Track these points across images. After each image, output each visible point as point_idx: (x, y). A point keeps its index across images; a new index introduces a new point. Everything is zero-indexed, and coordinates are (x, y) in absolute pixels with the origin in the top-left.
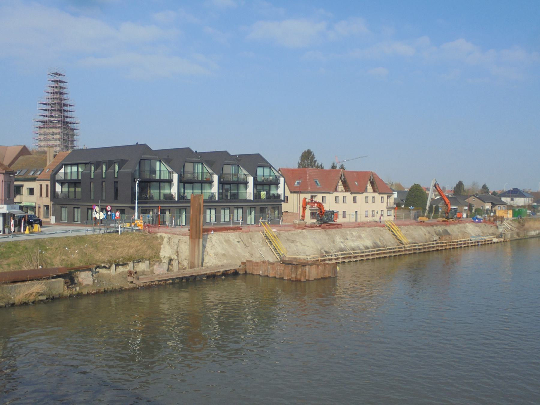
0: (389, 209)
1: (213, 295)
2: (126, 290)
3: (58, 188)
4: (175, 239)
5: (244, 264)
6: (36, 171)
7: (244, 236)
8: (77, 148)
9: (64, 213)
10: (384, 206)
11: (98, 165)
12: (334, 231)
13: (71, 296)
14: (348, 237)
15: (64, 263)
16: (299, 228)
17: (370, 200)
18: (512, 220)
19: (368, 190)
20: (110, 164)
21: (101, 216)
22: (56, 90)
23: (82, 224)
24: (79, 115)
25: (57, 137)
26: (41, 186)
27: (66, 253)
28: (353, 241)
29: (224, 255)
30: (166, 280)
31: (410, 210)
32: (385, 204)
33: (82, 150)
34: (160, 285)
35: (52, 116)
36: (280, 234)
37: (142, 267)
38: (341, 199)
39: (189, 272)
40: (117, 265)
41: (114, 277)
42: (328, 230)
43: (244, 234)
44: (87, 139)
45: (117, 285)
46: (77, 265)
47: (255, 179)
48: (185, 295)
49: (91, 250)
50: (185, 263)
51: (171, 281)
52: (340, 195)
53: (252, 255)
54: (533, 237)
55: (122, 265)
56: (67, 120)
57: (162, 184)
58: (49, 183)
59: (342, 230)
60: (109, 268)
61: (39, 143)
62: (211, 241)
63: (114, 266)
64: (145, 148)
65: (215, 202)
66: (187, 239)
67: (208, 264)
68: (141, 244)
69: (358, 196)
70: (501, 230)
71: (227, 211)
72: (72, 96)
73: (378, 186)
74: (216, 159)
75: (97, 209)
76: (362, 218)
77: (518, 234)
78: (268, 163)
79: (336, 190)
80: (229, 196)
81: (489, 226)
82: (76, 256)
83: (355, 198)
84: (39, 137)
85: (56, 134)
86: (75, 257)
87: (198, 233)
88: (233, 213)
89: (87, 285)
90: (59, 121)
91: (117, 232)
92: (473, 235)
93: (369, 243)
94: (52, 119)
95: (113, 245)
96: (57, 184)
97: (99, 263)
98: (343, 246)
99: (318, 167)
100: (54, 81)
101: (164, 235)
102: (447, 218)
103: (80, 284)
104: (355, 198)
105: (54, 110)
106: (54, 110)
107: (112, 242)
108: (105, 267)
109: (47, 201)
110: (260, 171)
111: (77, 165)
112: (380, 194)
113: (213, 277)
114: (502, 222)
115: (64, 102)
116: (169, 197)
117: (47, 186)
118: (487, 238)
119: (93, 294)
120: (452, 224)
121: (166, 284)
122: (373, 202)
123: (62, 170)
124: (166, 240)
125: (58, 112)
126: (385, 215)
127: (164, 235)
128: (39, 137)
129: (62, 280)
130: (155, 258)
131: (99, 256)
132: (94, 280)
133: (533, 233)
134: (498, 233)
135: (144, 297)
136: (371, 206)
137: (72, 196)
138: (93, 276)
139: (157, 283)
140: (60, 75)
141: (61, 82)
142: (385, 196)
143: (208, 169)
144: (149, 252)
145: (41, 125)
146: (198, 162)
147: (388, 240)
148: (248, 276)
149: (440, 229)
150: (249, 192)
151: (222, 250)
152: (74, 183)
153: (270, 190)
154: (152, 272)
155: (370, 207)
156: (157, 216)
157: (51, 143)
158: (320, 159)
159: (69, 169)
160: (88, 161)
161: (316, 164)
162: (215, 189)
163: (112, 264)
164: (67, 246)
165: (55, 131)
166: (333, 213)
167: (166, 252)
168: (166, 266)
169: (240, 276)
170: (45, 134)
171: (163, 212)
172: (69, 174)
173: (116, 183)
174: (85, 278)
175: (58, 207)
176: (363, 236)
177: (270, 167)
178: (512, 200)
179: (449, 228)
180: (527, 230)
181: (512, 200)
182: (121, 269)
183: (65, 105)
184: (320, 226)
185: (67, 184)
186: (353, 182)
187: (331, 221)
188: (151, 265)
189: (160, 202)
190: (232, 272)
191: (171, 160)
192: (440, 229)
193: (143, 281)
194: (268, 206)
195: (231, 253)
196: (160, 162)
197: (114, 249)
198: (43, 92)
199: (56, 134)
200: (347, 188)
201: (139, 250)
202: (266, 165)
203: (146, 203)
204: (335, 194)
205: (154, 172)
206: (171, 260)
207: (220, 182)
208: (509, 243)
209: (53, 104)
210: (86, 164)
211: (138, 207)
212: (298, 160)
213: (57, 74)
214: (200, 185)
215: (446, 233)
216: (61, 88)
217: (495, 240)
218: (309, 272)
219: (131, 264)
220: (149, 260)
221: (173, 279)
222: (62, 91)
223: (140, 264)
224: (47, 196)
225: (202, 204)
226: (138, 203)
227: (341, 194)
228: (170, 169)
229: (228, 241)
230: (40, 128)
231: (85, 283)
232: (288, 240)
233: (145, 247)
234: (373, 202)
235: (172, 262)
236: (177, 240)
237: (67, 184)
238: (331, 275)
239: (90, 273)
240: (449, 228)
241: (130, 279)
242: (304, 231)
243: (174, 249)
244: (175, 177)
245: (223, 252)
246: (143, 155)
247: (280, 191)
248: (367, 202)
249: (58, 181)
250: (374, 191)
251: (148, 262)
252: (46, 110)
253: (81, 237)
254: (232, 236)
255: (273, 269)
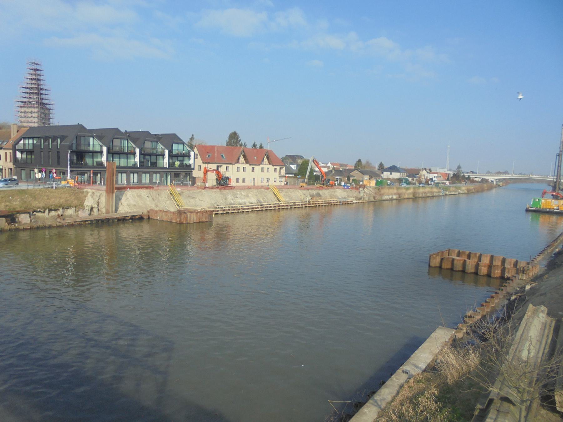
0: (281, 177)
1: (128, 233)
2: (54, 227)
3: (19, 155)
4: (97, 194)
5: (148, 212)
6: (3, 142)
7: (153, 193)
8: (52, 125)
9: (23, 173)
10: (277, 175)
11: (46, 139)
12: (227, 191)
13: (10, 230)
14: (238, 196)
15: (8, 207)
16: (201, 188)
17: (265, 170)
18: (373, 188)
19: (264, 163)
20: (54, 139)
21: (39, 176)
22: (34, 77)
23: (27, 181)
24: (53, 97)
25: (36, 115)
26: (6, 153)
27: (10, 201)
28: (241, 199)
29: (135, 205)
30: (86, 221)
31: (298, 178)
32: (278, 174)
33: (56, 126)
34: (81, 224)
35: (30, 98)
36: (183, 192)
37: (70, 212)
38: (241, 169)
39: (103, 216)
40: (50, 210)
41: (47, 219)
42: (222, 191)
43: (154, 191)
44: (61, 117)
45: (48, 223)
46: (18, 209)
47: (170, 152)
48: (103, 233)
49: (30, 199)
50: (104, 210)
51: (89, 222)
52: (265, 167)
53: (157, 206)
54: (387, 200)
55: (55, 210)
56: (44, 101)
57: (94, 154)
58: (11, 151)
59: (234, 191)
60: (44, 212)
61: (20, 119)
62: (126, 195)
63: (47, 211)
64: (81, 127)
65: (138, 168)
66: (105, 193)
67: (121, 212)
68: (70, 196)
69: (256, 167)
70: (362, 195)
71: (148, 175)
72: (48, 82)
73: (271, 159)
74: (138, 138)
75: (36, 170)
76: (258, 183)
77: (374, 198)
78: (181, 140)
79: (238, 161)
80: (149, 163)
81: (354, 191)
82: (18, 203)
83: (253, 169)
84: (21, 114)
85: (34, 112)
86: (16, 204)
87: (115, 190)
88: (152, 177)
89: (26, 223)
90: (37, 102)
91: (53, 187)
92: (340, 197)
93: (254, 200)
94: (31, 100)
95: (48, 196)
96: (17, 152)
97: (35, 209)
98: (232, 202)
99: (241, 145)
100: (32, 69)
101: (89, 190)
102: (323, 185)
103: (19, 223)
104: (275, 169)
105: (32, 93)
106: (32, 93)
107: (46, 194)
108: (40, 211)
109: (11, 165)
110: (175, 146)
111: (33, 138)
112: (273, 166)
113: (123, 220)
114: (364, 189)
115: (41, 87)
116: (100, 164)
117: (10, 153)
118: (350, 200)
119: (28, 229)
120: (325, 189)
121: (86, 224)
122: (238, 179)
123: (22, 142)
124: (90, 194)
125: (37, 94)
126: (278, 181)
127: (89, 190)
128: (21, 114)
129: (4, 219)
130: (80, 206)
131: (35, 204)
132: (31, 221)
133: (387, 197)
134: (360, 197)
135: (71, 233)
136: (268, 175)
137: (29, 161)
138: (30, 217)
139: (79, 223)
140: (37, 64)
141: (38, 70)
142: (278, 168)
143: (131, 144)
144: (75, 202)
145: (22, 104)
146: (124, 139)
147: (269, 200)
148: (151, 220)
149: (314, 192)
150: (165, 162)
151: (131, 202)
152: (30, 152)
153: (183, 161)
154: (77, 216)
155: (265, 175)
156: (90, 177)
157: (30, 120)
158: (243, 139)
159: (27, 141)
160: (39, 136)
161: (240, 143)
162: (137, 159)
163: (46, 209)
164: (11, 196)
165: (33, 110)
166: (228, 178)
167: (89, 202)
168: (87, 212)
169: (145, 220)
170: (25, 112)
171: (95, 174)
172: (27, 145)
173: (58, 152)
174: (24, 219)
175: (19, 169)
176: (250, 195)
177: (183, 143)
178: (391, 174)
179: (321, 192)
180: (381, 195)
181: (391, 174)
182: (53, 213)
183: (41, 89)
184: (218, 188)
185: (25, 153)
186: (257, 155)
187: (226, 184)
188: (76, 211)
189: (93, 167)
190: (138, 217)
191: (261, 144)
192: (314, 192)
193: (68, 221)
194: (181, 173)
195: (141, 204)
196: (93, 138)
197: (48, 199)
198: (23, 77)
199: (34, 112)
200: (247, 161)
201: (68, 200)
202: (179, 141)
203: (81, 168)
204: (237, 165)
205: (89, 145)
206: (92, 208)
207: (141, 154)
208: (367, 204)
209: (32, 88)
210: (39, 138)
211: (71, 171)
212: (227, 139)
213: (35, 63)
214: (125, 156)
215: (319, 195)
216: (38, 75)
217: (355, 201)
218: (190, 218)
219: (61, 210)
220: (75, 207)
221: (91, 221)
222: (39, 77)
223: (69, 210)
224: (11, 161)
225: (115, 170)
226: (70, 167)
227: (242, 164)
228: (101, 144)
229: (139, 196)
230: (21, 107)
231: (24, 222)
232: (189, 196)
233: (73, 198)
234: (238, 179)
235: (94, 209)
236: (99, 195)
237: (25, 153)
238: (207, 220)
239: (28, 215)
240: (321, 192)
241: (59, 220)
242: (203, 191)
243: (95, 200)
244: (105, 149)
245: (134, 203)
246: (80, 133)
247: (191, 161)
248: (262, 171)
249: (19, 150)
250: (270, 164)
251: (74, 209)
252: (25, 93)
253: (23, 190)
254: (144, 193)
255: (166, 215)
